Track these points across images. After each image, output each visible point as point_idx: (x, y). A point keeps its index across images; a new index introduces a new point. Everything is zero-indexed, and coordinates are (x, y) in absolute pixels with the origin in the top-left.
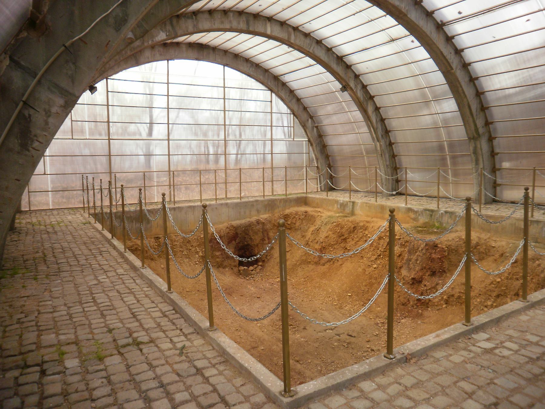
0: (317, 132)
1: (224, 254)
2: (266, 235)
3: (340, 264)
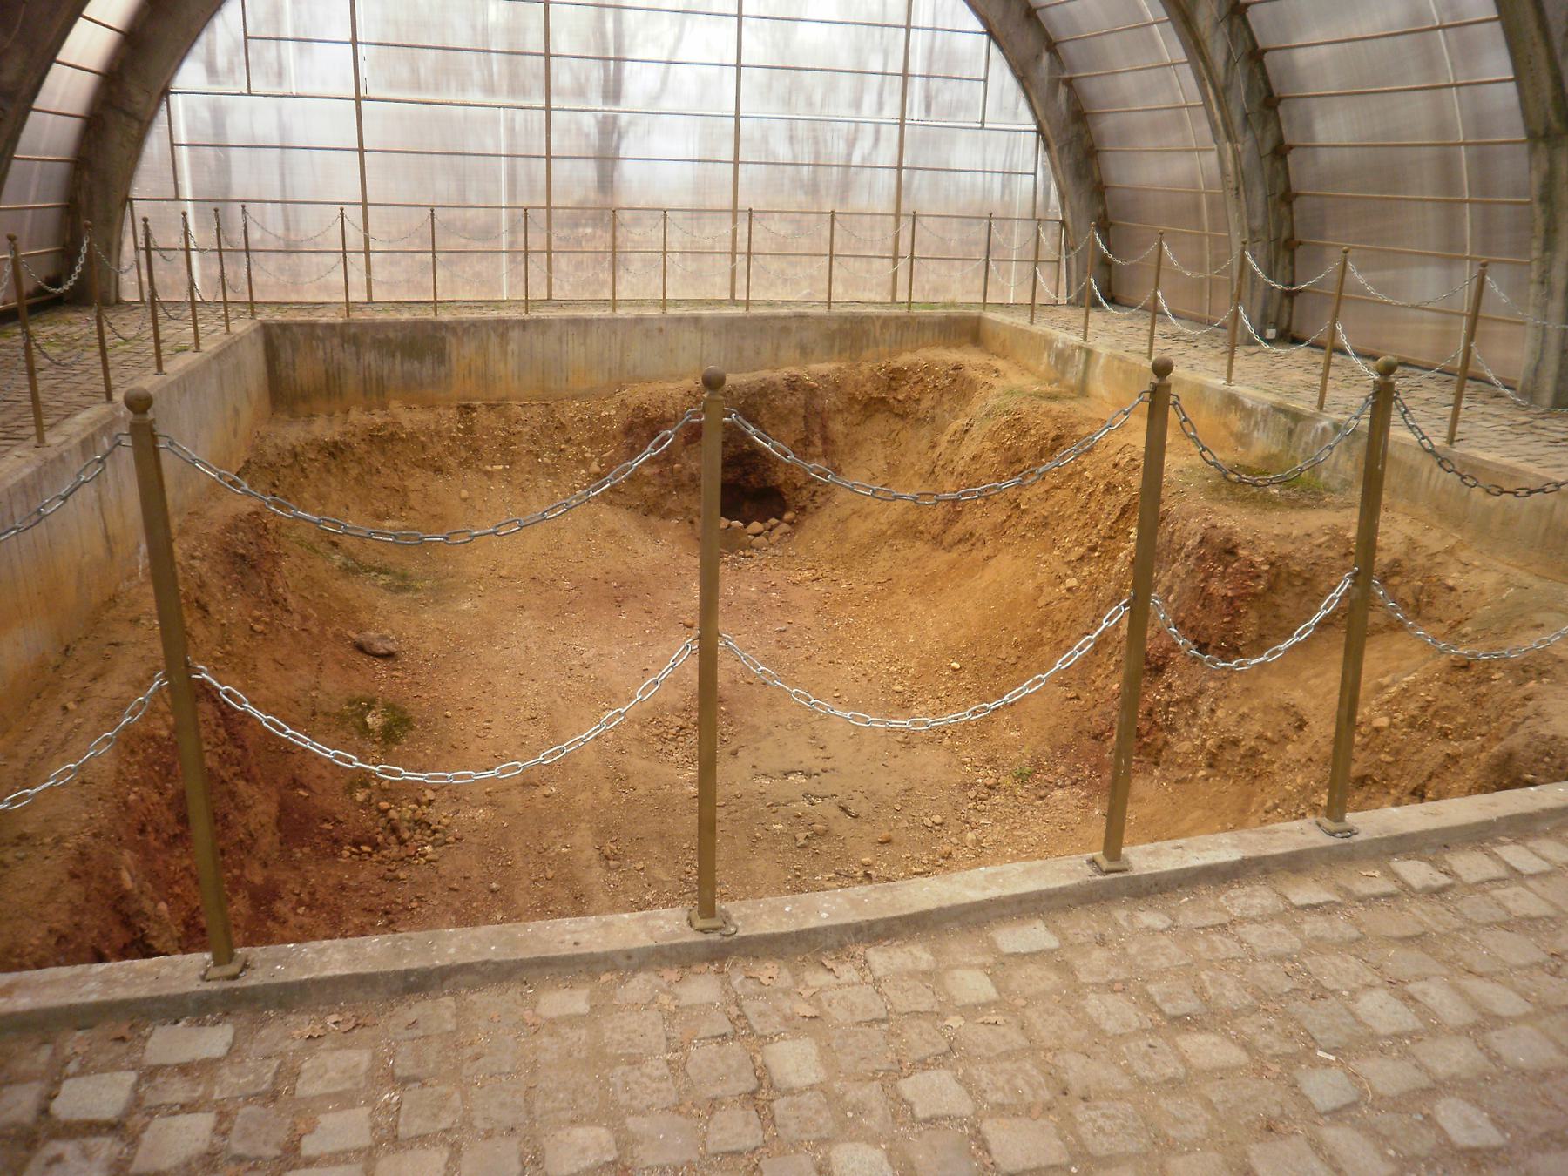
0: (1068, 99)
1: (668, 474)
2: (817, 429)
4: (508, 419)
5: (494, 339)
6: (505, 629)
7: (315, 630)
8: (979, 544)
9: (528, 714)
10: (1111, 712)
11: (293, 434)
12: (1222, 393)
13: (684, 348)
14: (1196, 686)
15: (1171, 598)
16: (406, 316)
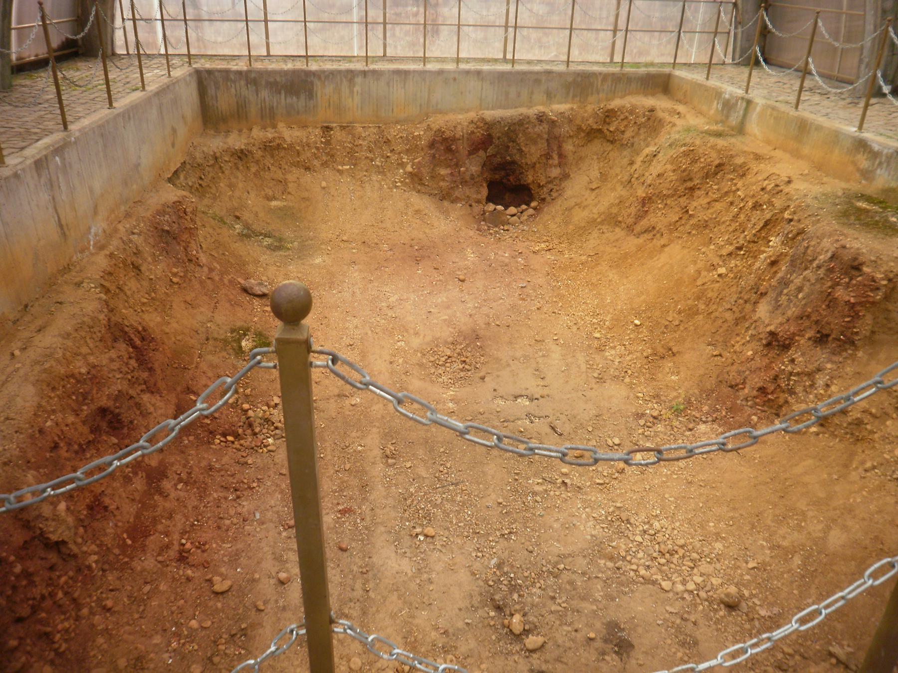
2: (555, 148)
3: (662, 243)
4: (354, 136)
5: (345, 83)
6: (341, 277)
7: (217, 278)
8: (658, 235)
9: (349, 341)
10: (744, 372)
11: (216, 144)
12: (854, 138)
13: (470, 92)
14: (816, 364)
15: (800, 296)
16: (289, 66)
